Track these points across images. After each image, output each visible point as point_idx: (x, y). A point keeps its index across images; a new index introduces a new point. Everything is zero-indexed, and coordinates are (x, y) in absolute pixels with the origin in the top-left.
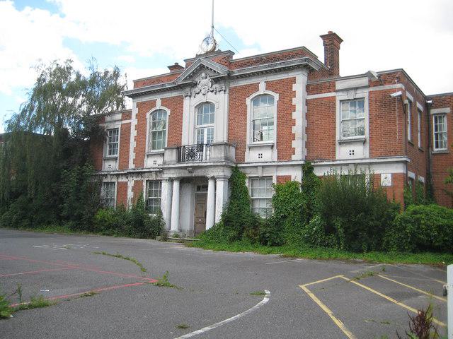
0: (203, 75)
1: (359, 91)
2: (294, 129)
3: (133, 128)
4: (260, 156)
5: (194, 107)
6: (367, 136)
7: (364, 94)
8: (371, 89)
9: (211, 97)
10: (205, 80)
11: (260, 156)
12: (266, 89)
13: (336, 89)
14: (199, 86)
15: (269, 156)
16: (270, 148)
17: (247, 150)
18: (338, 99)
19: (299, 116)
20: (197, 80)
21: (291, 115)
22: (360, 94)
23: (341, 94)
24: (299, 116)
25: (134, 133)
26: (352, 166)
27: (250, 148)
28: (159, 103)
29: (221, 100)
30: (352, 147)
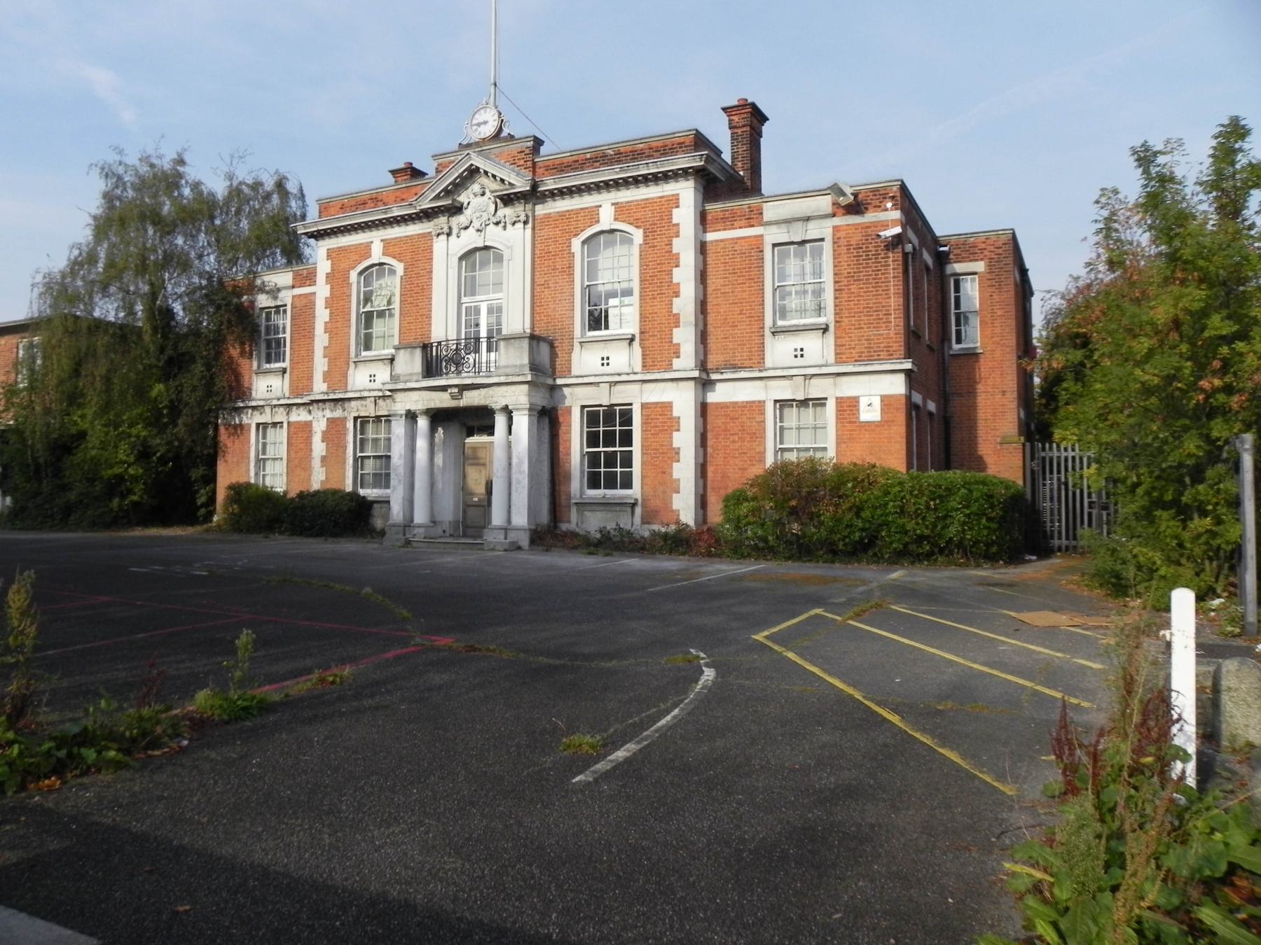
8: (837, 221)
12: (616, 219)
17: (577, 347)
19: (685, 275)
20: (463, 198)
21: (670, 273)
22: (813, 230)
23: (774, 229)
25: (322, 315)
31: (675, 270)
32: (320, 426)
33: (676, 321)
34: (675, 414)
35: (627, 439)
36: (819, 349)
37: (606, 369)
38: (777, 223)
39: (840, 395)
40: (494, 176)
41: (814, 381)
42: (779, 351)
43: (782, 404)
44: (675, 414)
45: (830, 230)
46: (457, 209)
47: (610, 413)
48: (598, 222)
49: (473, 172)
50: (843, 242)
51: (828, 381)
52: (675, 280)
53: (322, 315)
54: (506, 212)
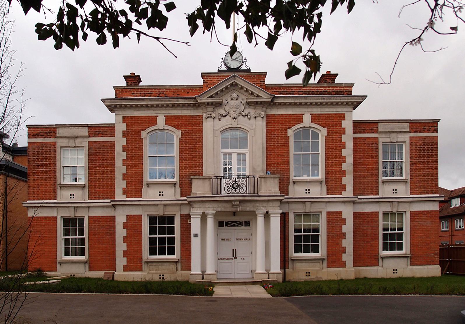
0: (234, 95)
1: (79, 140)
2: (344, 167)
3: (118, 148)
4: (308, 191)
5: (219, 132)
6: (176, 179)
7: (406, 138)
8: (412, 135)
9: (242, 122)
10: (234, 102)
11: (395, 191)
12: (166, 124)
13: (379, 130)
14: (227, 108)
15: (318, 192)
16: (319, 184)
17: (291, 184)
18: (58, 145)
19: (348, 152)
20: (224, 99)
21: (341, 151)
22: (401, 138)
23: (383, 135)
24: (348, 152)
25: (120, 156)
26: (396, 203)
27: (294, 183)
28: (307, 119)
29: (256, 128)
30: (394, 187)
31: (343, 150)
32: (121, 219)
33: (344, 174)
34: (343, 217)
35: (171, 231)
36: (403, 191)
37: (161, 198)
38: (385, 133)
39: (412, 210)
40: (247, 91)
41: (400, 204)
42: (385, 191)
43: (385, 214)
44: (343, 217)
45: (409, 139)
46: (219, 105)
47: (162, 219)
48: (156, 124)
49: (234, 85)
50: (414, 144)
51: (407, 205)
52: (343, 155)
53: (120, 156)
54: (251, 111)
